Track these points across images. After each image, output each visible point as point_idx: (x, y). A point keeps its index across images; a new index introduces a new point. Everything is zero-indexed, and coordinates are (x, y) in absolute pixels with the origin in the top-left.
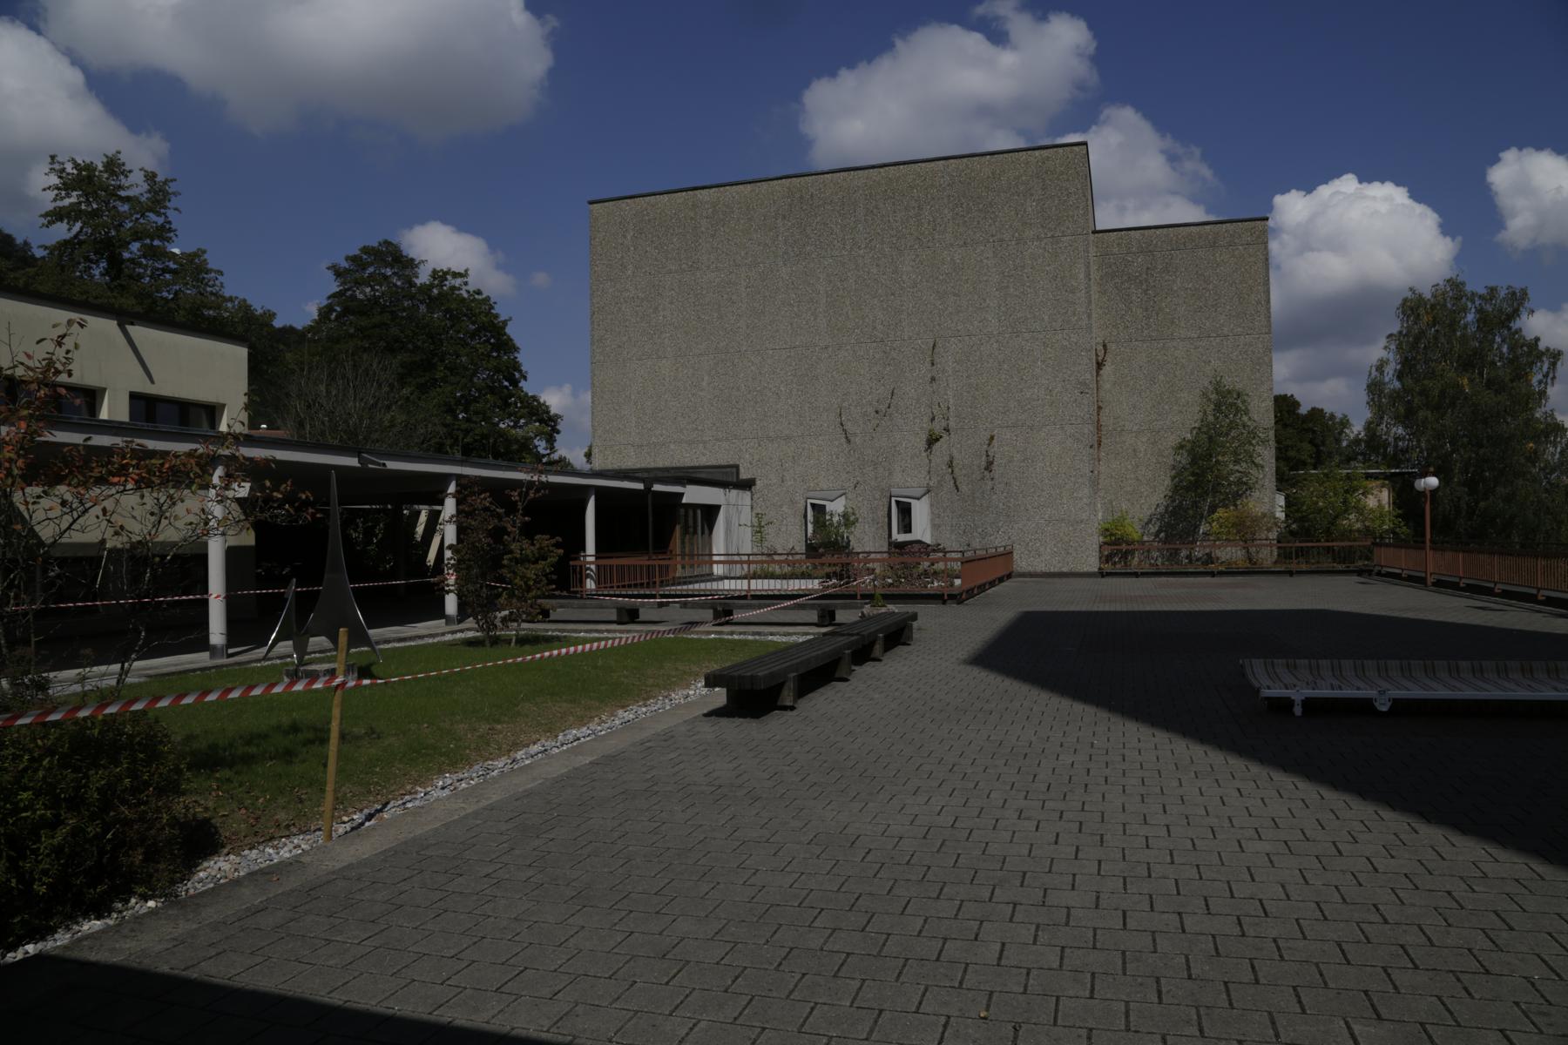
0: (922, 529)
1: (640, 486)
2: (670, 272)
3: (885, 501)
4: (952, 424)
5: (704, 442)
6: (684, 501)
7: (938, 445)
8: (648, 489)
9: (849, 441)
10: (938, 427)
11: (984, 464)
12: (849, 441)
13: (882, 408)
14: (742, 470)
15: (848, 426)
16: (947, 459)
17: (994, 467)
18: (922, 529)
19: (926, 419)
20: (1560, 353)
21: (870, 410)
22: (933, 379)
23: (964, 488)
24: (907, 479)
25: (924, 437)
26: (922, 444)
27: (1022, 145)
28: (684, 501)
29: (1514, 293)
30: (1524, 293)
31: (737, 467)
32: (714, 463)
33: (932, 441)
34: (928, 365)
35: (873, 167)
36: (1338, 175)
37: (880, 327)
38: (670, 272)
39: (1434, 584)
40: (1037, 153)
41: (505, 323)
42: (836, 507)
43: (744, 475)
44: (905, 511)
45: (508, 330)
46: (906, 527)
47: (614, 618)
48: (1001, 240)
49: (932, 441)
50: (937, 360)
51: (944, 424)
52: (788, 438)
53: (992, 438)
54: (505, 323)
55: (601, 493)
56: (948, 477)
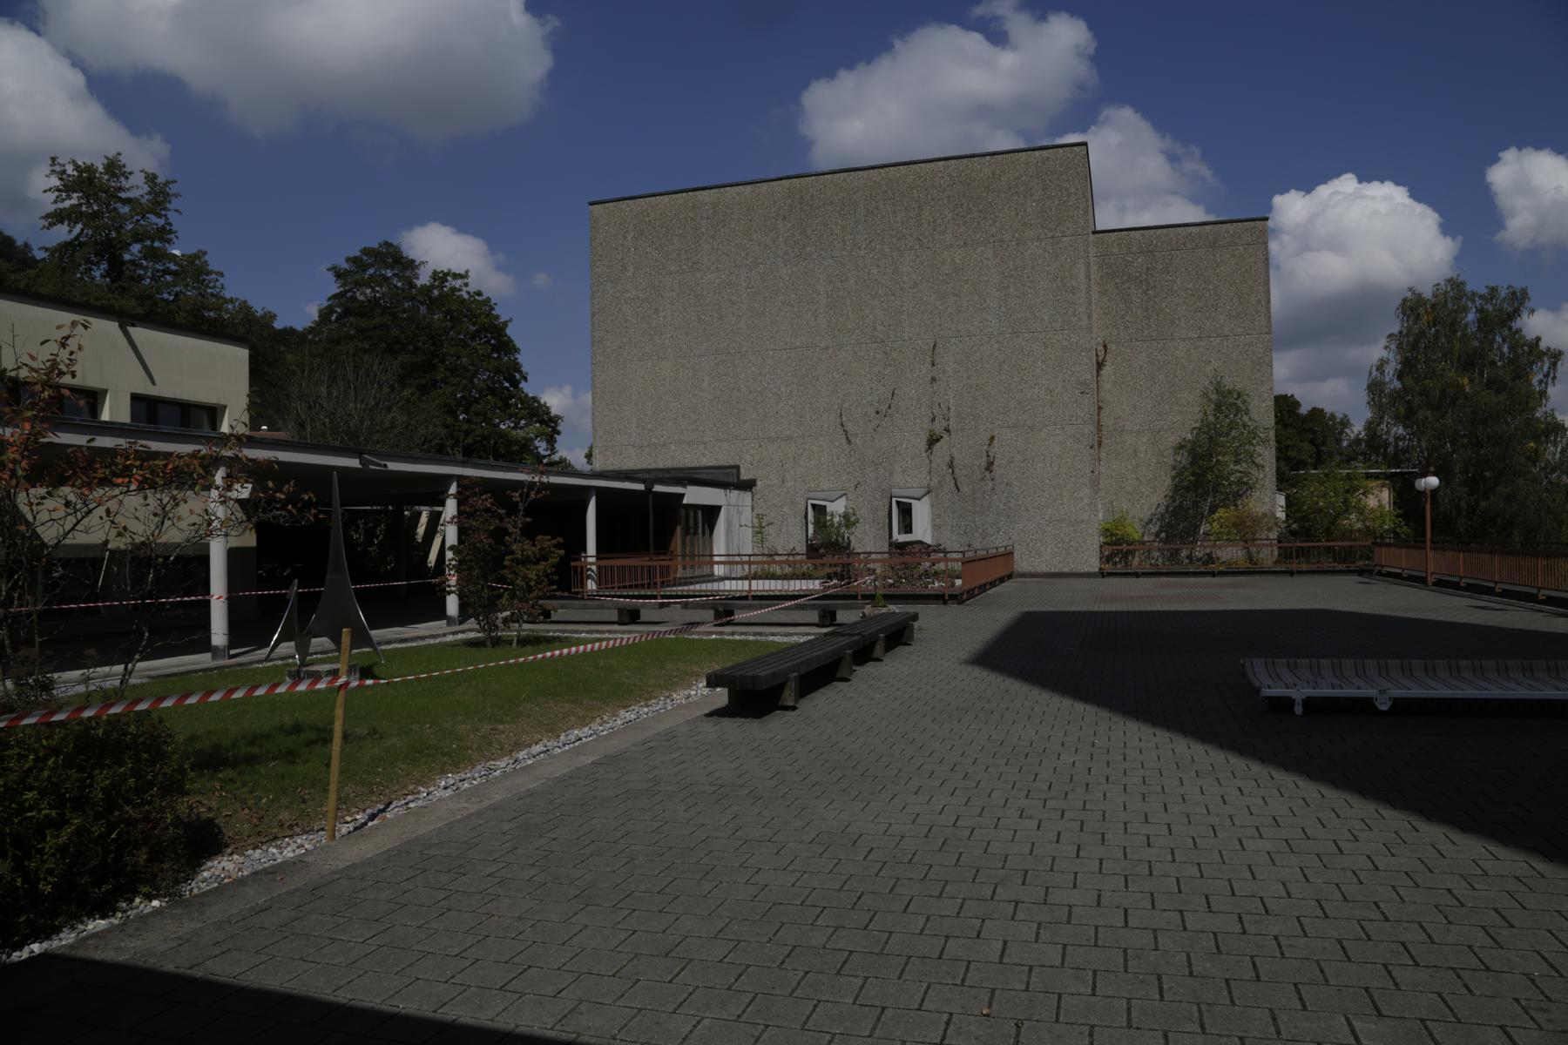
0: (922, 529)
1: (641, 487)
2: (670, 273)
3: (886, 501)
4: (953, 424)
5: (705, 443)
6: (685, 501)
7: (938, 445)
8: (649, 490)
9: (849, 442)
10: (938, 427)
11: (984, 464)
12: (849, 442)
13: (883, 408)
14: (742, 471)
15: (849, 427)
16: (947, 459)
17: (995, 468)
18: (922, 529)
20: (1560, 353)
21: (871, 410)
22: (933, 379)
23: (965, 489)
24: (907, 482)
25: (925, 437)
26: (923, 445)
28: (685, 501)
29: (1514, 293)
31: (738, 468)
32: (715, 463)
33: (933, 441)
35: (873, 168)
37: (880, 328)
38: (670, 273)
39: (1434, 584)
41: (505, 324)
42: (837, 508)
43: (745, 476)
44: (906, 511)
45: (508, 331)
46: (907, 528)
47: (615, 618)
48: (1002, 241)
49: (933, 441)
50: (937, 361)
51: (944, 424)
52: (789, 439)
53: (992, 438)
54: (505, 324)
55: (602, 494)
56: (949, 478)
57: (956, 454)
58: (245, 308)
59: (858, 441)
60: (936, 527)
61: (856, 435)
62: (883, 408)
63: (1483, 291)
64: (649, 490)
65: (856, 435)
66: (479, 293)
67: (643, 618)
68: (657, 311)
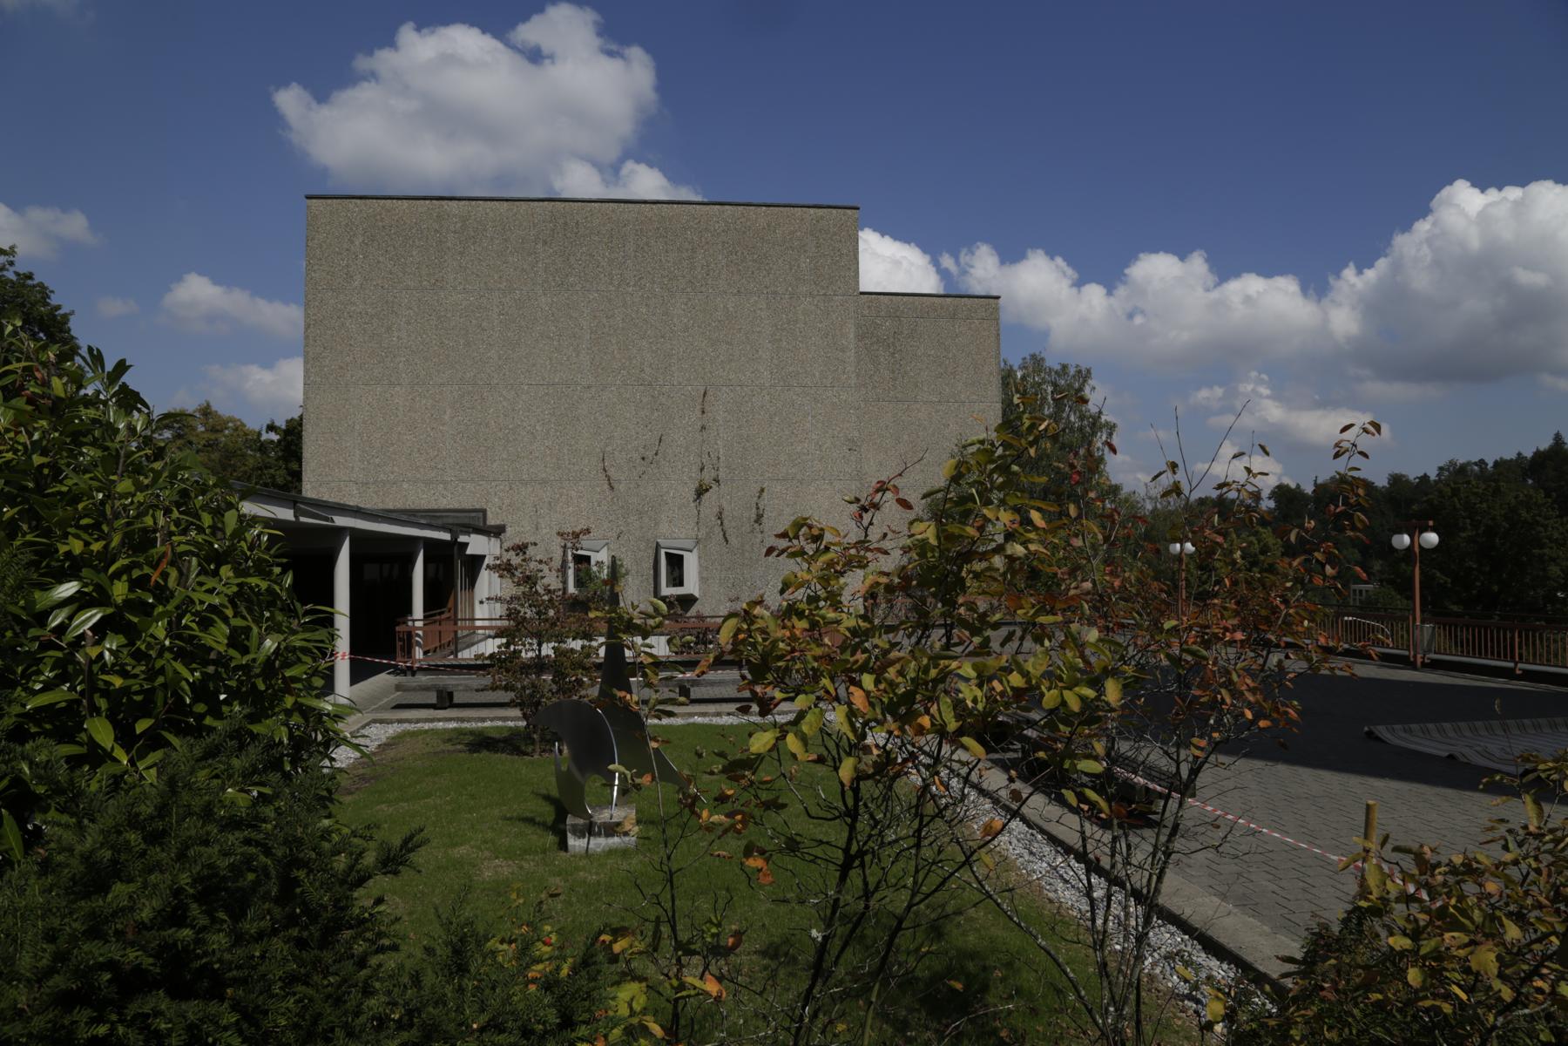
0: (691, 585)
1: (446, 536)
2: (407, 288)
3: (652, 552)
4: (722, 475)
5: (445, 483)
6: (469, 551)
7: (707, 495)
8: (455, 539)
9: (612, 488)
10: (708, 476)
11: (754, 516)
12: (612, 488)
13: (650, 454)
14: (489, 515)
15: (612, 472)
16: (716, 510)
17: (764, 520)
18: (691, 585)
19: (695, 469)
20: (1115, 426)
21: (636, 456)
22: (703, 428)
23: (733, 540)
24: (675, 535)
25: (693, 486)
26: (692, 495)
27: (699, 199)
28: (469, 551)
29: (1080, 372)
30: (1089, 371)
31: (484, 512)
32: (457, 506)
33: (701, 492)
34: (699, 413)
35: (645, 202)
36: (1281, 273)
37: (648, 370)
38: (407, 288)
40: (812, 211)
43: (492, 521)
44: (676, 562)
45: (71, 324)
46: (678, 580)
47: (434, 701)
48: (775, 293)
49: (701, 492)
50: (707, 408)
51: (713, 474)
52: (544, 482)
55: (358, 537)
56: (717, 529)
57: (725, 505)
58: (1396, 480)
59: (622, 487)
60: (703, 580)
61: (619, 481)
62: (650, 454)
63: (1057, 367)
64: (455, 539)
65: (619, 481)
66: (30, 276)
67: (456, 700)
68: (389, 329)
